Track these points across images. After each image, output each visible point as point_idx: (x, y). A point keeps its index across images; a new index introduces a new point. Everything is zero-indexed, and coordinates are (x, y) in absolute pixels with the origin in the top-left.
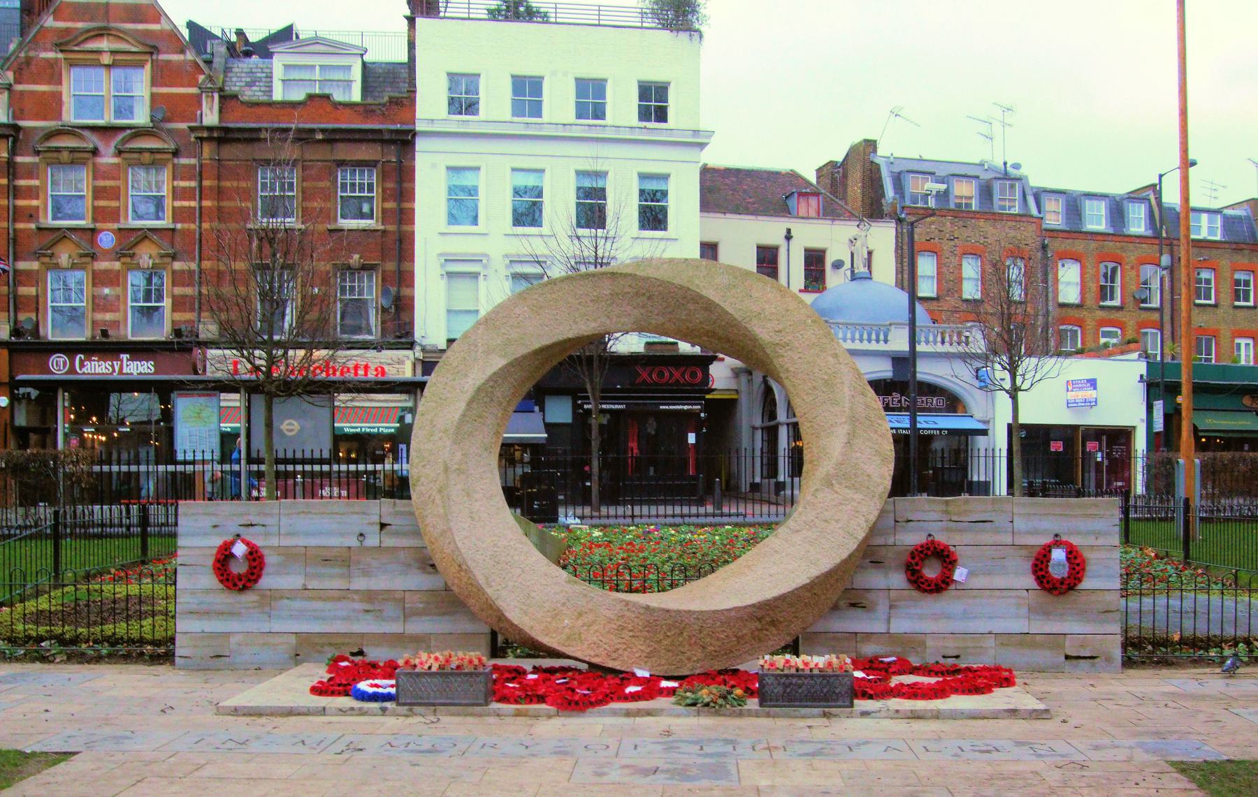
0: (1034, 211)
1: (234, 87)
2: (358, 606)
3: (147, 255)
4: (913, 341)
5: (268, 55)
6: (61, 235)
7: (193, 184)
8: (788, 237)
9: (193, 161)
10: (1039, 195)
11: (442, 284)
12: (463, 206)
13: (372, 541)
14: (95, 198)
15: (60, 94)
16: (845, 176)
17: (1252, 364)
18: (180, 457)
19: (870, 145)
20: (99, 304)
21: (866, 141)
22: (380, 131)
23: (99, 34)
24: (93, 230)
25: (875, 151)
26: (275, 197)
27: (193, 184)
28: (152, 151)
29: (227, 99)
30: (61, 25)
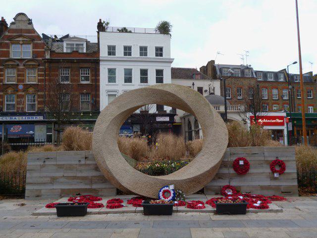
0: (255, 77)
1: (54, 49)
2: (79, 181)
3: (31, 90)
4: (226, 109)
5: (63, 41)
6: (9, 86)
7: (43, 73)
8: (193, 84)
9: (43, 67)
10: (256, 72)
11: (107, 97)
12: (112, 77)
13: (83, 162)
14: (18, 76)
15: (9, 51)
16: (207, 69)
17: (313, 112)
18: (36, 141)
19: (213, 62)
20: (18, 103)
21: (212, 61)
22: (91, 60)
23: (19, 36)
24: (17, 85)
25: (214, 63)
26: (64, 77)
27: (43, 73)
28: (33, 65)
29: (52, 53)
30: (9, 34)
